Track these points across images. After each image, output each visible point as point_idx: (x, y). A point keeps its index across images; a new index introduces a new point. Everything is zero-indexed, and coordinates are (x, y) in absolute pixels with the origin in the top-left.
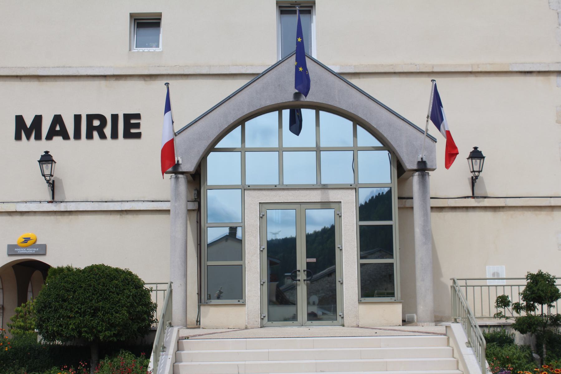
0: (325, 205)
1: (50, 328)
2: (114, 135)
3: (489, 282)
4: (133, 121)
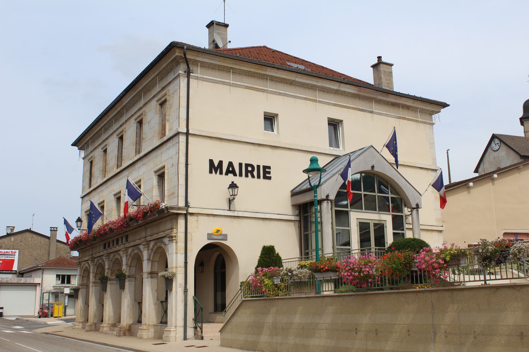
2: (259, 177)
4: (267, 170)
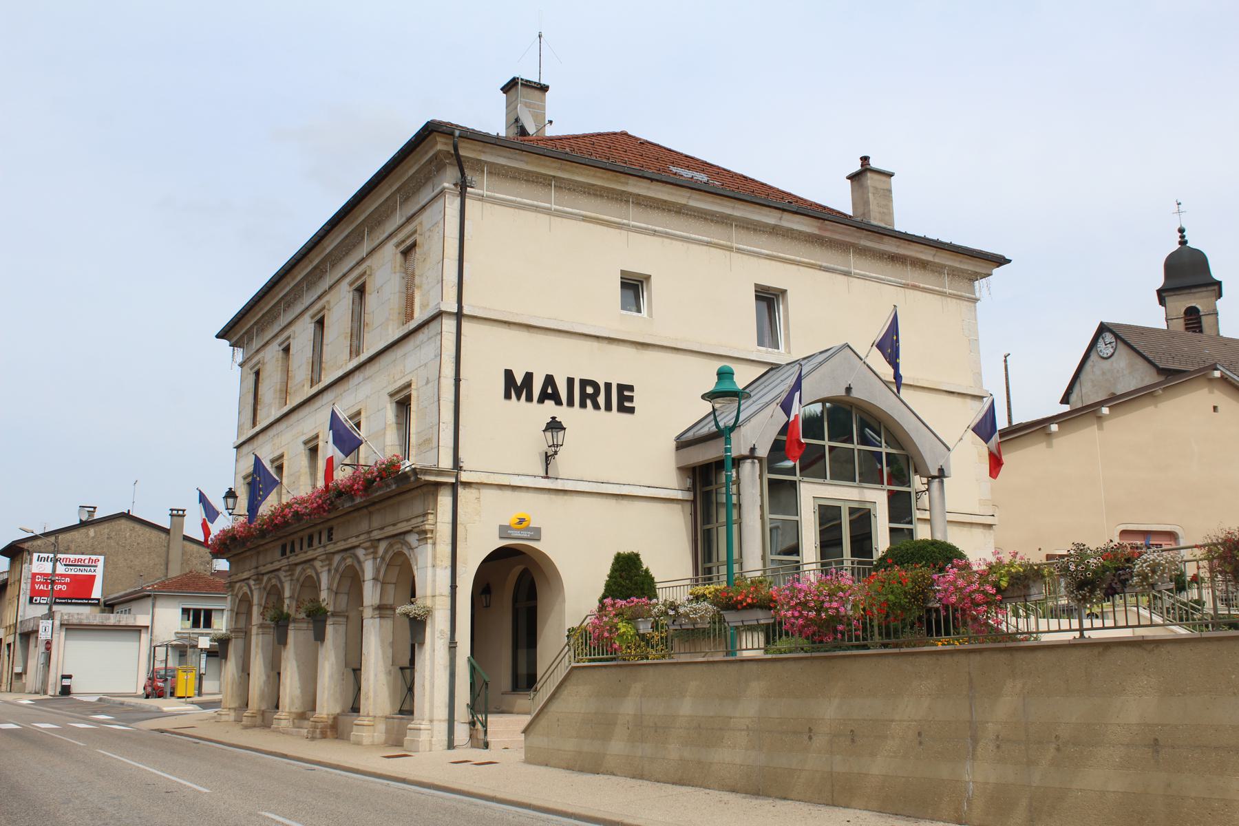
2: (608, 407)
4: (626, 393)
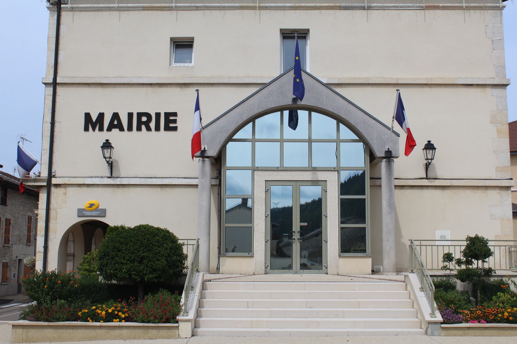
0: (315, 183)
1: (108, 271)
2: (157, 129)
3: (437, 243)
4: (171, 118)
